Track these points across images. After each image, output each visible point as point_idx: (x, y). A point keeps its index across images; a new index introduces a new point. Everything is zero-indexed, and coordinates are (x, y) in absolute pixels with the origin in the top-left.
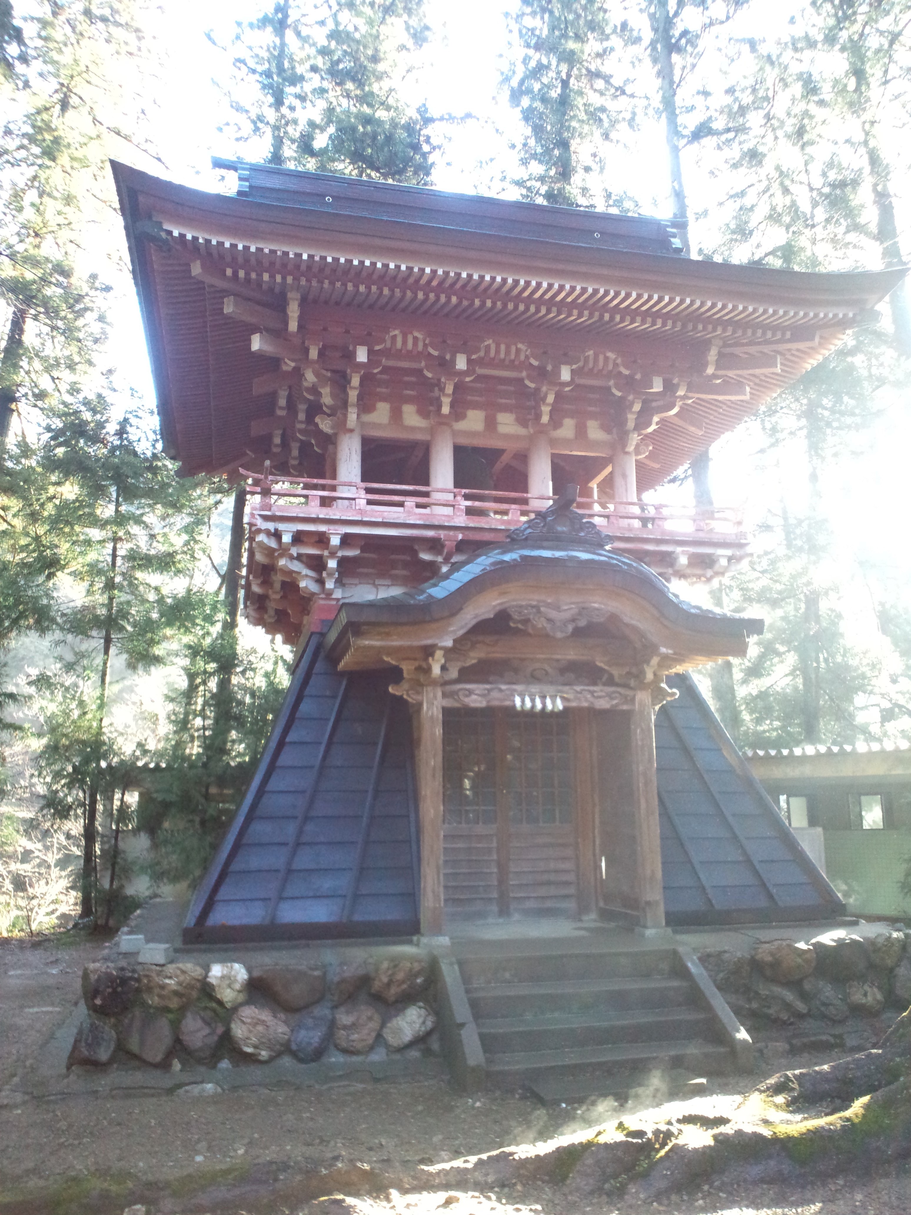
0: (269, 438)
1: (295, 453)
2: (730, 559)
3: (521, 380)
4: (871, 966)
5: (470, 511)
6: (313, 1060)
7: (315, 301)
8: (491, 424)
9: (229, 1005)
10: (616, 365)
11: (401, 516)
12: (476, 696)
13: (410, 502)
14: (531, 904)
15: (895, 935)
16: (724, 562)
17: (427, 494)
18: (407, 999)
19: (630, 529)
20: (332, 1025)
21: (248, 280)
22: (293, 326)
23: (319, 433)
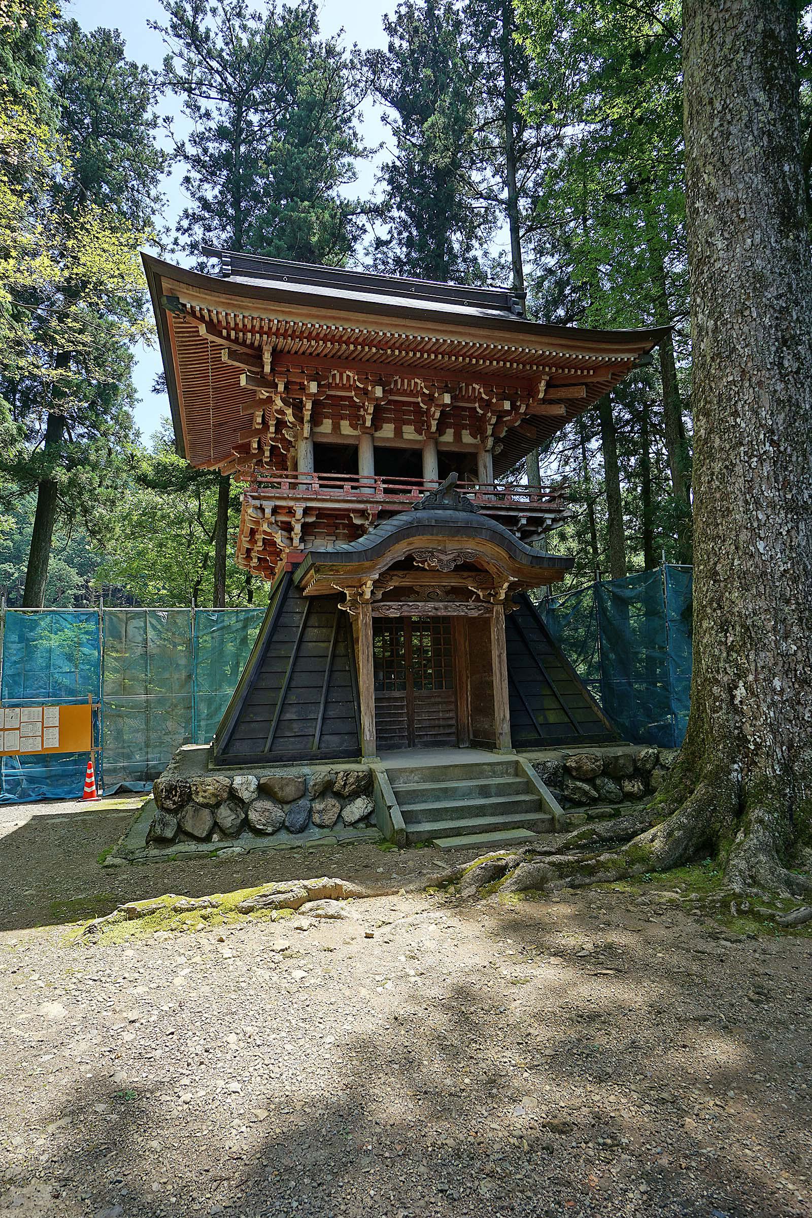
0: (249, 445)
1: (267, 454)
2: (554, 520)
3: (418, 403)
4: (636, 769)
5: (386, 491)
6: (299, 832)
7: (281, 351)
8: (398, 432)
9: (247, 801)
10: (480, 393)
11: (339, 498)
12: (393, 610)
13: (347, 485)
14: (429, 739)
15: (651, 751)
16: (549, 522)
17: (357, 480)
18: (355, 795)
19: (489, 501)
20: (311, 811)
21: (237, 338)
22: (267, 369)
23: (284, 440)
